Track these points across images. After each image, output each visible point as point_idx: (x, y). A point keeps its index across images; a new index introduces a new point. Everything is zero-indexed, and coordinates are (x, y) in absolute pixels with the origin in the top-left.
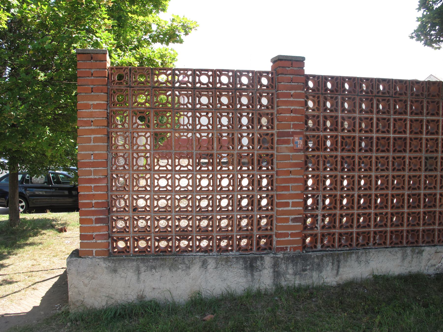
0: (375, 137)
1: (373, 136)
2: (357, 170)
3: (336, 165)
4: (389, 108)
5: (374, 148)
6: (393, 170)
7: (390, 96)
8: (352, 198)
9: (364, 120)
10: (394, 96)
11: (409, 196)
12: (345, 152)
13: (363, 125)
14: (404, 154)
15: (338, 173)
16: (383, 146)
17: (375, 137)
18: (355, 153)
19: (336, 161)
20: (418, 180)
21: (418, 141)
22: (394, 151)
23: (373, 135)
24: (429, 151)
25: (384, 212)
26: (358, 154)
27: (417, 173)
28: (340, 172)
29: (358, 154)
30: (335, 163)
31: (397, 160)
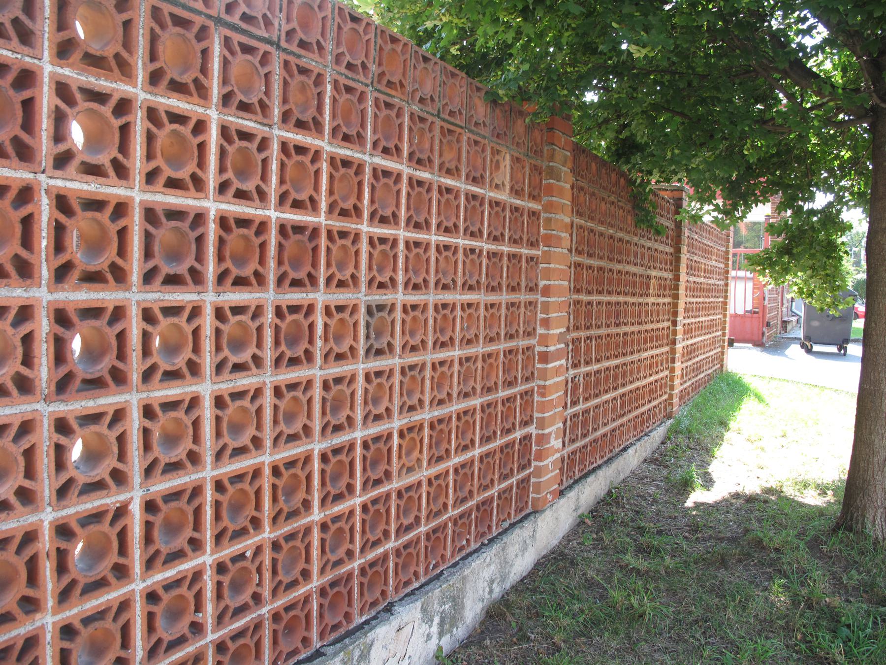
0: (212, 214)
1: (208, 210)
2: (135, 377)
3: (28, 361)
4: (267, 93)
5: (211, 269)
6: (62, 386)
7: (269, 42)
8: (118, 527)
9: (83, 104)
10: (283, 44)
11: (63, 531)
12: (75, 289)
13: (77, 134)
14: (311, 296)
15: (40, 406)
16: (174, 256)
17: (212, 214)
18: (128, 289)
19: (28, 340)
20: (113, 435)
21: (185, 225)
22: (61, 273)
23: (205, 204)
24: (160, 279)
25: (247, 547)
26: (141, 297)
27: (107, 401)
28: (47, 400)
29: (141, 297)
30: (20, 351)
31: (165, 323)
